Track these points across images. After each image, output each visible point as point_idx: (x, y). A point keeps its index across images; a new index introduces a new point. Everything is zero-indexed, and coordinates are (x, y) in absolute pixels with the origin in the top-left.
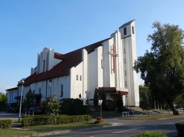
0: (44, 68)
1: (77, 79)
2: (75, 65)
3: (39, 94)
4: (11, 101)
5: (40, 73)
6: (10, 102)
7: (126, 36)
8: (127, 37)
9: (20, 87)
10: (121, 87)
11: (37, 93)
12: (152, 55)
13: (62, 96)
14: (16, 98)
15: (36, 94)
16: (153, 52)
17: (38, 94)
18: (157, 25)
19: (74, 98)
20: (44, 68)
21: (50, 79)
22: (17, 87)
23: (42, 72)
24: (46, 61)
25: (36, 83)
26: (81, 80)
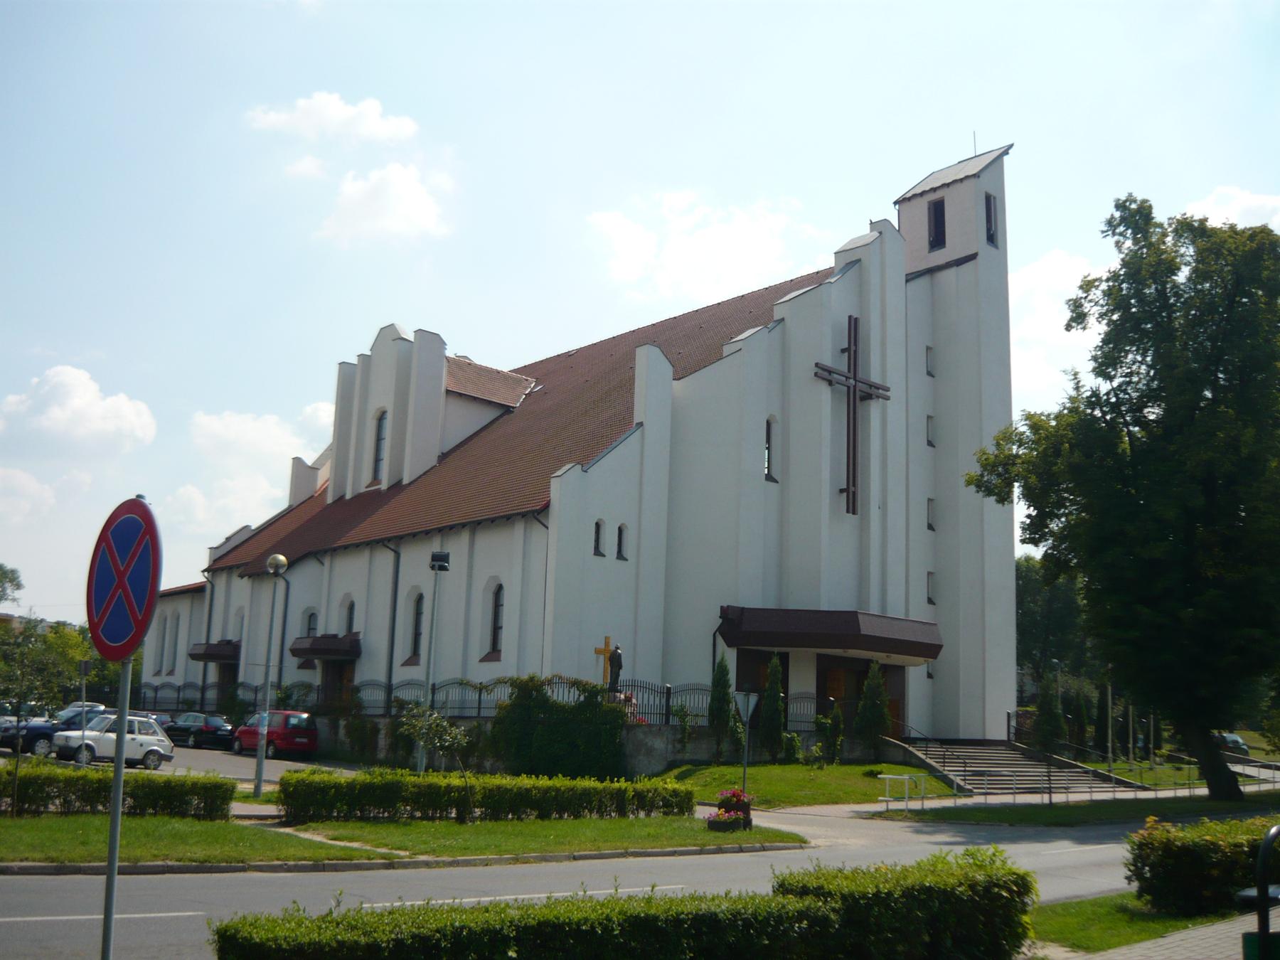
0: (377, 460)
1: (598, 552)
2: (587, 454)
3: (342, 633)
4: (164, 672)
5: (348, 496)
6: (158, 673)
7: (940, 257)
8: (948, 265)
9: (221, 582)
10: (897, 600)
11: (332, 631)
12: (1095, 399)
13: (494, 653)
14: (201, 651)
15: (325, 637)
16: (1105, 387)
17: (335, 636)
18: (1134, 218)
19: (255, 523)
20: (377, 460)
21: (435, 546)
22: (198, 578)
23: (363, 490)
24: (389, 417)
25: (327, 561)
26: (620, 556)
